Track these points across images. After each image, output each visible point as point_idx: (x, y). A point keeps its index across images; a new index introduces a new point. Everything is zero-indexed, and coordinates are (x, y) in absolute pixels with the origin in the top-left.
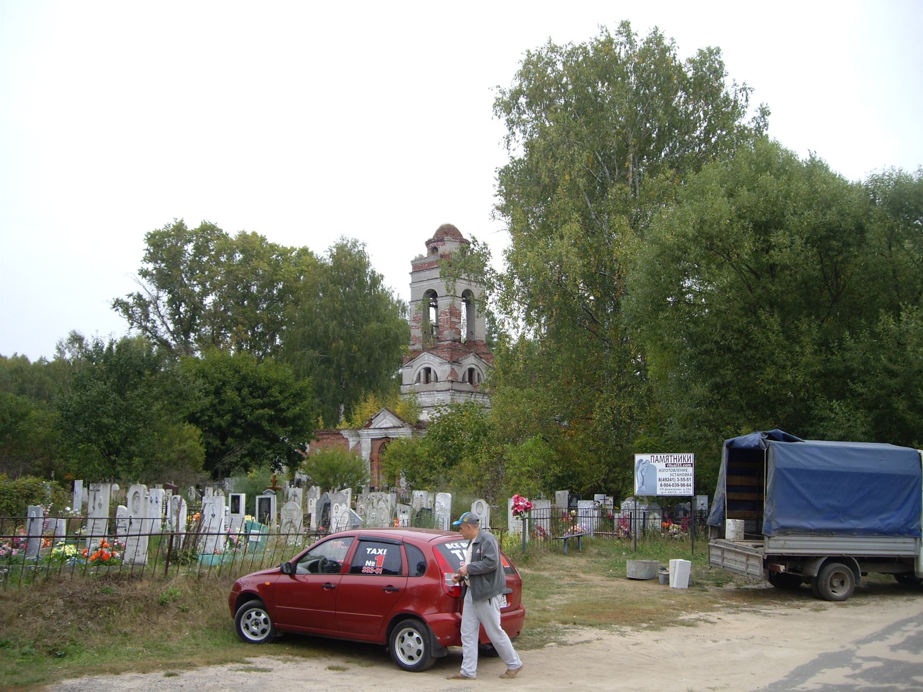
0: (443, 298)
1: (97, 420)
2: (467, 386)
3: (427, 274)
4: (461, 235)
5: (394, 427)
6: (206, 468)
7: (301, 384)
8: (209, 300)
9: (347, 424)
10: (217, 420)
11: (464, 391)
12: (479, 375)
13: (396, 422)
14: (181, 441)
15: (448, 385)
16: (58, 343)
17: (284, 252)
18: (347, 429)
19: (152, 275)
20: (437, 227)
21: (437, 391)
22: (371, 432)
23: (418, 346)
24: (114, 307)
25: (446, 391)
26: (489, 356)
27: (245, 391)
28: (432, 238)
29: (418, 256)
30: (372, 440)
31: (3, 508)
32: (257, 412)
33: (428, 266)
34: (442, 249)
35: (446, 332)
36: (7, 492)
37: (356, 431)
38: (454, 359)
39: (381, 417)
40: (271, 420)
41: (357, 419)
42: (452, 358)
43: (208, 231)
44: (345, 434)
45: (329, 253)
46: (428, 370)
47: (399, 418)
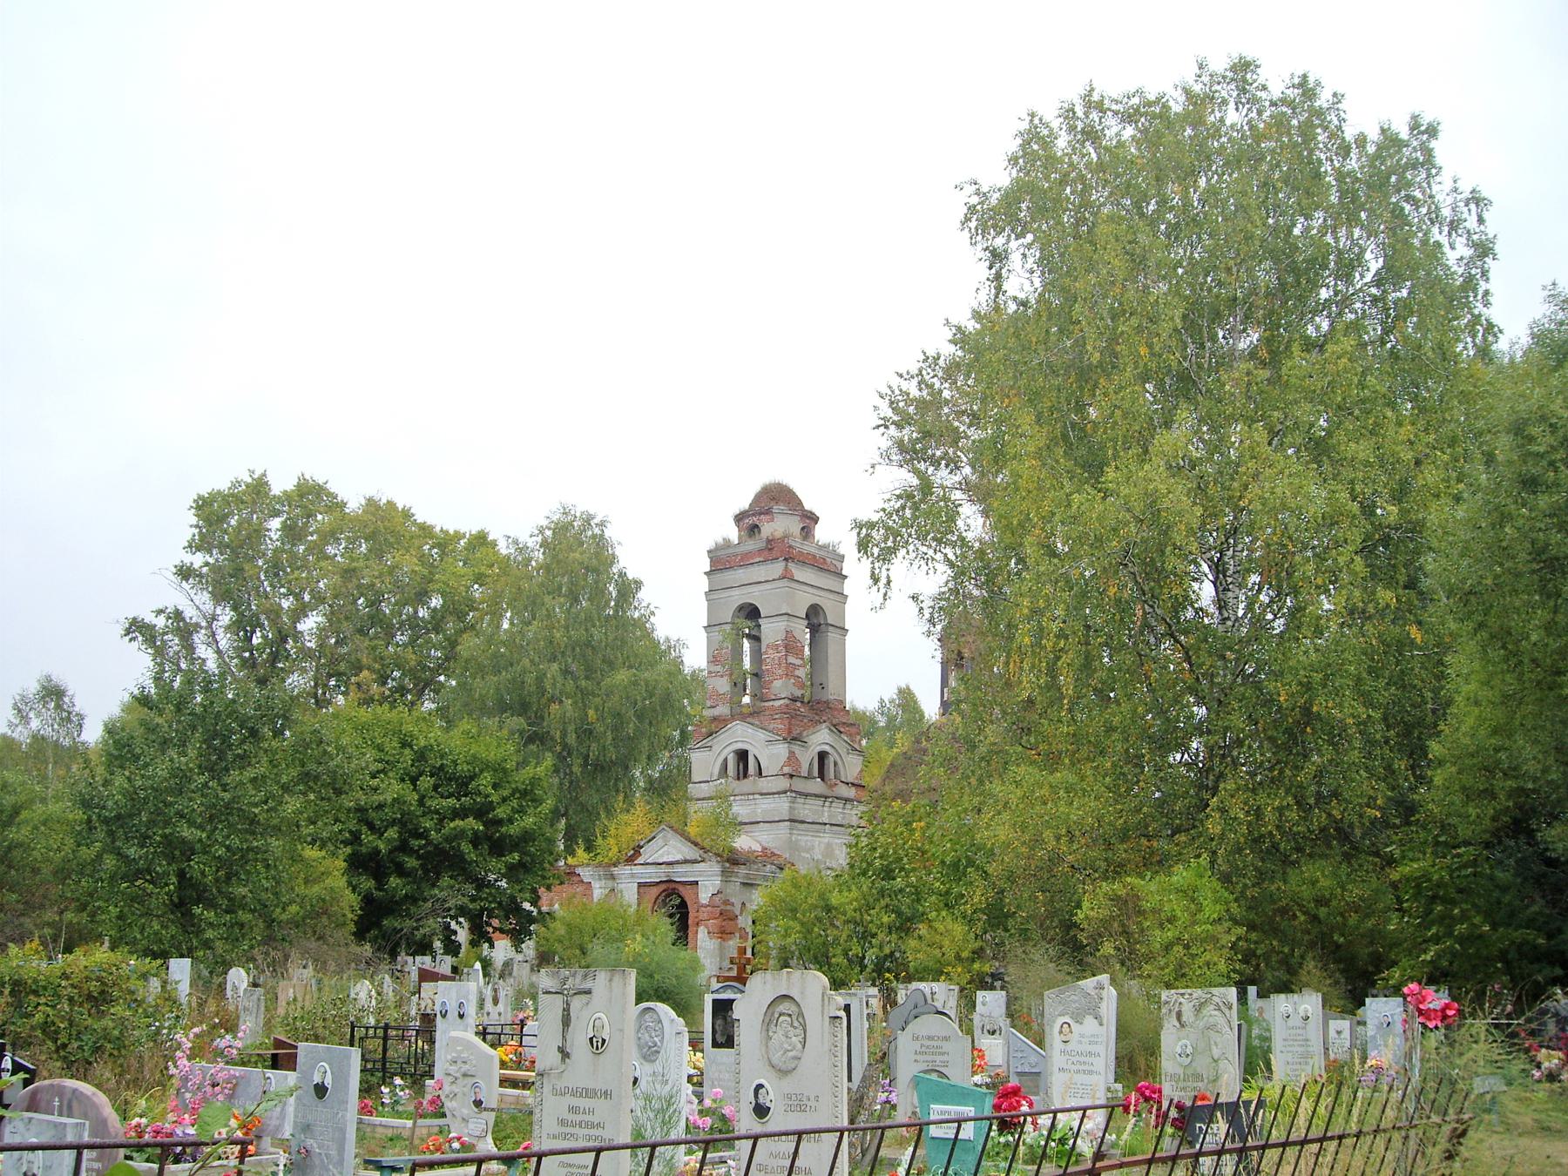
0: (771, 620)
1: (167, 831)
2: (816, 786)
3: (741, 575)
4: (800, 503)
5: (686, 862)
6: (360, 935)
7: (528, 772)
8: (310, 624)
9: (586, 855)
10: (367, 838)
11: (811, 795)
12: (836, 764)
13: (690, 852)
14: (306, 882)
15: (784, 783)
16: (18, 697)
17: (445, 542)
18: (588, 865)
19: (201, 576)
20: (757, 488)
21: (762, 794)
22: (637, 870)
23: (723, 710)
24: (128, 632)
25: (778, 793)
26: (853, 730)
27: (426, 782)
28: (747, 507)
29: (720, 541)
30: (640, 885)
31: (33, 1028)
32: (452, 825)
33: (742, 560)
34: (769, 528)
35: (777, 684)
36: (45, 988)
37: (608, 869)
38: (795, 733)
39: (659, 841)
40: (476, 841)
41: (610, 847)
42: (790, 732)
43: (310, 495)
44: (586, 874)
45: (539, 539)
46: (742, 756)
47: (696, 844)
